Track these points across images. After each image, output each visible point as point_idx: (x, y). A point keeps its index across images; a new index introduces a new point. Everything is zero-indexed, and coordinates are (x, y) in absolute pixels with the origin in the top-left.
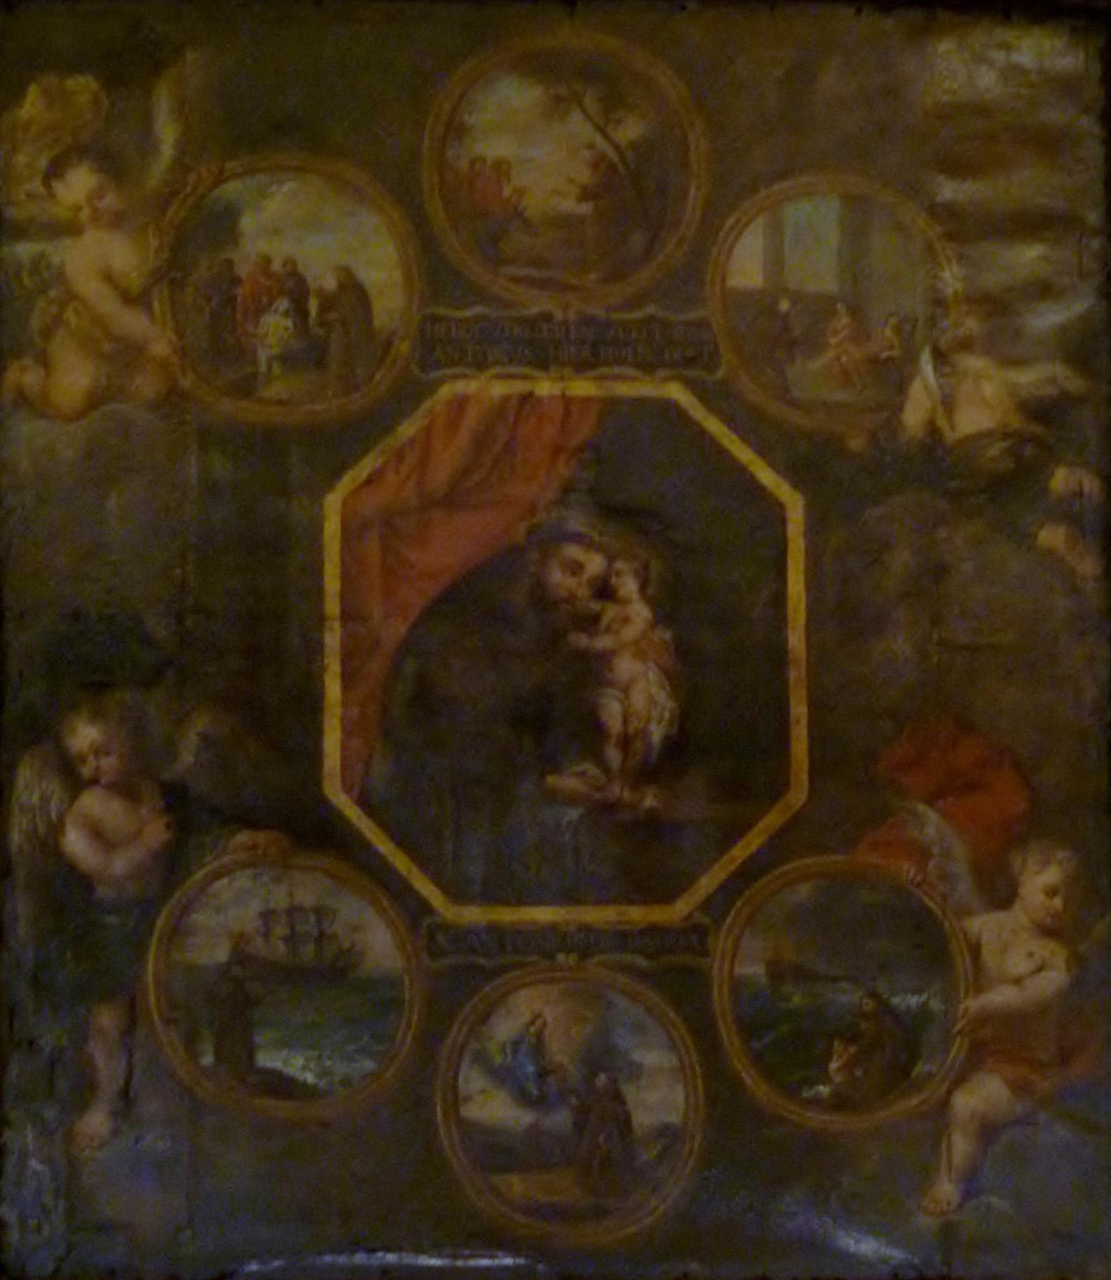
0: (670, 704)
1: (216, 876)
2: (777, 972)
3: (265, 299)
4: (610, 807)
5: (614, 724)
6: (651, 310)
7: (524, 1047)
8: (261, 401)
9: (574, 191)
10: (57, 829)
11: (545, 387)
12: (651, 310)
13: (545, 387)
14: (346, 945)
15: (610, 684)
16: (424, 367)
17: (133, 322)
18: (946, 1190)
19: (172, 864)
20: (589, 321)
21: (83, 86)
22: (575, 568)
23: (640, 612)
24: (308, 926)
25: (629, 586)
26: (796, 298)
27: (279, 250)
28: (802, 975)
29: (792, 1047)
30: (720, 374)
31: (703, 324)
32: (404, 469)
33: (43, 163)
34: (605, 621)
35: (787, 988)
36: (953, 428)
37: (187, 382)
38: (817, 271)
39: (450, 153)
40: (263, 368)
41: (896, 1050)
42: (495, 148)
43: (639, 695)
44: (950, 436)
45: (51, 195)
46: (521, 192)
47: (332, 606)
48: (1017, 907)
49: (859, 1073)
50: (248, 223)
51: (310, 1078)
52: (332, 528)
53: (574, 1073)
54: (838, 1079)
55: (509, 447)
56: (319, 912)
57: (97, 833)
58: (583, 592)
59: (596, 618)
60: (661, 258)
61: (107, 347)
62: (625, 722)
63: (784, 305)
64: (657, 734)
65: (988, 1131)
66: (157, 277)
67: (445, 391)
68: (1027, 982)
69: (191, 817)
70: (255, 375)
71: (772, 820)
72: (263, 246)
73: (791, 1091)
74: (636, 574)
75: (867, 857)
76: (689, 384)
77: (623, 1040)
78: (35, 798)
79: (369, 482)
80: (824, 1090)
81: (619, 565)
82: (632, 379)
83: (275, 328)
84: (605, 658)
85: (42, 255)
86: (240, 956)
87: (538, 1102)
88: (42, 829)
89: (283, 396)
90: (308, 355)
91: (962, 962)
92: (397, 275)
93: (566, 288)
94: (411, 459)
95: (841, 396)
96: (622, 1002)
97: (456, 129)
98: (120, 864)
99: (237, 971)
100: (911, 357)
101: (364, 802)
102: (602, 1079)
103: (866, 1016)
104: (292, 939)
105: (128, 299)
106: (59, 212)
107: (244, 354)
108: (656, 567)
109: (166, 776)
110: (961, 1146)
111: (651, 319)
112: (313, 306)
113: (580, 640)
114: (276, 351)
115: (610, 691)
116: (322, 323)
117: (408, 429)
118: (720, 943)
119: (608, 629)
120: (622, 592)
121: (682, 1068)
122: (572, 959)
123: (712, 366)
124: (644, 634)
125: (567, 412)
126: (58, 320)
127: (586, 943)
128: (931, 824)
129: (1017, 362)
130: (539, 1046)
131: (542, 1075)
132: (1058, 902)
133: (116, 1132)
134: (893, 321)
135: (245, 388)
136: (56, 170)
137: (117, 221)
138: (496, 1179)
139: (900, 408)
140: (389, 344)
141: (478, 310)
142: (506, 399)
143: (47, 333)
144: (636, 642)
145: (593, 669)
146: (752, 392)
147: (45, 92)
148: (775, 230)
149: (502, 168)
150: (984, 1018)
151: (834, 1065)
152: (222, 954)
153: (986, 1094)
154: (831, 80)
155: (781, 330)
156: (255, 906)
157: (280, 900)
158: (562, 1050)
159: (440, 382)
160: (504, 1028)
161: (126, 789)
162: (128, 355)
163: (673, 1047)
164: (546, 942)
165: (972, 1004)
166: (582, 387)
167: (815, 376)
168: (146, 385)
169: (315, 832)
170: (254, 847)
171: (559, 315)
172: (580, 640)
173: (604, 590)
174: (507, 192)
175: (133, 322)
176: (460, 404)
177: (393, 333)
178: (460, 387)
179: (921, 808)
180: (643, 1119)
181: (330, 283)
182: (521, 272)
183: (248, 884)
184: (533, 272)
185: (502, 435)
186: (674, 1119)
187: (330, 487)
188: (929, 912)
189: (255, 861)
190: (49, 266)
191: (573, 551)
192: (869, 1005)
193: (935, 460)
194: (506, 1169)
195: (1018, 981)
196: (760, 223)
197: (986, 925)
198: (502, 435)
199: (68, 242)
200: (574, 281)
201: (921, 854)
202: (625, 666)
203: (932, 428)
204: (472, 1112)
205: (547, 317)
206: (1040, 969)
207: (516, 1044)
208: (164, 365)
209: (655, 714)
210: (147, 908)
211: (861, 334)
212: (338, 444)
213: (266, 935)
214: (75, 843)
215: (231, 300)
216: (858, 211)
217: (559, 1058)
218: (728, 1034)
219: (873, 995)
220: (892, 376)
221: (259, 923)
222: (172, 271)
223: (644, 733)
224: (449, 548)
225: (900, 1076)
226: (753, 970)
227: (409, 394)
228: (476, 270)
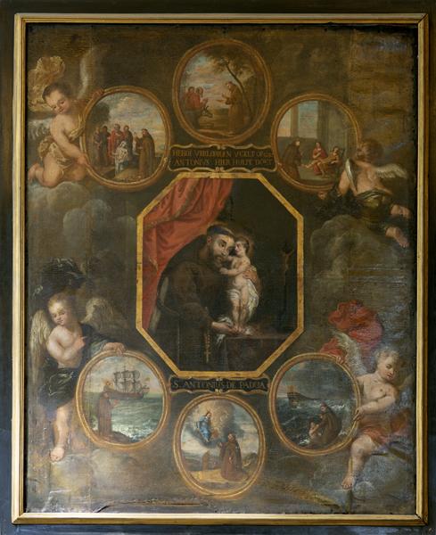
0: (256, 295)
1: (99, 359)
2: (292, 397)
3: (118, 142)
4: (236, 334)
5: (236, 303)
6: (250, 145)
7: (204, 424)
8: (116, 180)
9: (225, 100)
10: (45, 341)
11: (213, 175)
12: (250, 145)
13: (213, 175)
14: (143, 385)
15: (235, 288)
16: (173, 167)
17: (73, 150)
18: (350, 479)
19: (85, 355)
20: (228, 149)
21: (57, 60)
22: (223, 244)
23: (246, 260)
24: (130, 379)
25: (241, 251)
26: (302, 140)
27: (123, 123)
28: (300, 397)
29: (295, 423)
30: (274, 170)
31: (269, 151)
32: (165, 207)
33: (43, 89)
34: (233, 263)
35: (295, 403)
36: (357, 189)
37: (91, 173)
38: (309, 130)
39: (182, 85)
40: (117, 168)
41: (332, 425)
42: (198, 84)
43: (245, 292)
44: (356, 193)
45: (46, 102)
46: (206, 100)
47: (140, 259)
48: (377, 372)
49: (320, 434)
50: (112, 112)
51: (130, 435)
52: (140, 229)
53: (221, 435)
54: (312, 437)
55: (201, 196)
56: (134, 373)
57: (59, 343)
58: (226, 253)
59: (230, 262)
60: (255, 126)
61: (64, 160)
62: (240, 302)
63: (298, 143)
64: (251, 306)
65: (365, 457)
66: (81, 133)
67: (180, 176)
68: (380, 400)
69: (90, 335)
70: (114, 170)
71: (291, 339)
72: (117, 121)
73: (295, 441)
74: (245, 246)
75: (322, 353)
76: (264, 174)
77: (238, 421)
78: (39, 330)
79: (152, 211)
80: (307, 441)
81: (239, 243)
82: (245, 172)
83: (121, 153)
84: (233, 277)
85: (42, 124)
86: (108, 390)
87: (206, 444)
88: (41, 342)
89: (125, 179)
90: (132, 163)
91: (357, 393)
92: (164, 132)
93: (221, 137)
94: (167, 202)
95: (318, 178)
96: (237, 407)
97: (184, 77)
98: (67, 355)
99: (106, 395)
100: (342, 164)
101: (149, 332)
102: (230, 436)
103: (323, 414)
104: (125, 383)
105: (71, 141)
106: (49, 109)
107: (111, 163)
108: (251, 244)
109: (82, 322)
110: (355, 462)
111: (252, 149)
112: (134, 143)
113: (225, 271)
114: (122, 161)
115: (235, 290)
116: (138, 151)
117: (166, 191)
118: (272, 386)
119: (234, 267)
120: (239, 253)
121: (258, 433)
122: (221, 391)
123: (272, 166)
124: (247, 269)
125: (231, 199)
126: (47, 150)
127: (225, 384)
128: (346, 341)
129: (380, 165)
130: (209, 423)
131: (209, 435)
132: (391, 370)
133: (64, 456)
134: (336, 150)
135: (111, 175)
136: (47, 93)
137: (68, 112)
138: (193, 474)
139: (338, 183)
140: (160, 158)
141: (191, 145)
142: (201, 179)
143: (44, 154)
144: (244, 272)
145: (226, 283)
146: (287, 178)
147: (44, 62)
148: (295, 113)
149: (200, 91)
150: (365, 413)
151: (311, 432)
152: (101, 390)
153: (364, 443)
154: (315, 56)
155: (296, 152)
156: (112, 371)
157: (121, 369)
158: (217, 425)
159: (178, 173)
160: (198, 416)
161: (69, 327)
162: (71, 162)
163: (255, 425)
164: (211, 385)
165: (361, 409)
166: (226, 175)
167: (307, 170)
168: (77, 174)
169: (133, 343)
170: (112, 349)
171: (219, 148)
172: (225, 271)
173: (233, 252)
174: (201, 101)
175: (73, 150)
176: (185, 181)
177: (161, 155)
178: (184, 175)
179: (343, 335)
180: (244, 452)
181: (140, 136)
182: (206, 131)
183: (110, 362)
184: (211, 131)
185: (199, 193)
186: (255, 451)
187: (139, 213)
188: (345, 374)
189: (113, 353)
190: (45, 128)
191: (223, 237)
192: (324, 409)
193: (351, 203)
194: (196, 470)
195: (376, 400)
196: (289, 113)
197: (366, 379)
198: (199, 193)
199: (50, 120)
200: (223, 134)
201: (342, 352)
202: (240, 281)
203: (349, 191)
204: (185, 448)
205: (214, 148)
206: (385, 396)
207: (201, 423)
208: (84, 167)
209: (251, 299)
210: (76, 372)
211: (324, 155)
212: (142, 197)
213: (116, 382)
214: (52, 347)
215: (106, 142)
216: (325, 106)
217: (216, 428)
218: (274, 420)
219: (325, 405)
220: (336, 169)
221: (114, 377)
222: (85, 132)
223: (246, 307)
224: (178, 239)
225: (334, 437)
226: (283, 396)
227: (166, 178)
228: (192, 132)
